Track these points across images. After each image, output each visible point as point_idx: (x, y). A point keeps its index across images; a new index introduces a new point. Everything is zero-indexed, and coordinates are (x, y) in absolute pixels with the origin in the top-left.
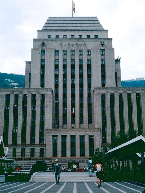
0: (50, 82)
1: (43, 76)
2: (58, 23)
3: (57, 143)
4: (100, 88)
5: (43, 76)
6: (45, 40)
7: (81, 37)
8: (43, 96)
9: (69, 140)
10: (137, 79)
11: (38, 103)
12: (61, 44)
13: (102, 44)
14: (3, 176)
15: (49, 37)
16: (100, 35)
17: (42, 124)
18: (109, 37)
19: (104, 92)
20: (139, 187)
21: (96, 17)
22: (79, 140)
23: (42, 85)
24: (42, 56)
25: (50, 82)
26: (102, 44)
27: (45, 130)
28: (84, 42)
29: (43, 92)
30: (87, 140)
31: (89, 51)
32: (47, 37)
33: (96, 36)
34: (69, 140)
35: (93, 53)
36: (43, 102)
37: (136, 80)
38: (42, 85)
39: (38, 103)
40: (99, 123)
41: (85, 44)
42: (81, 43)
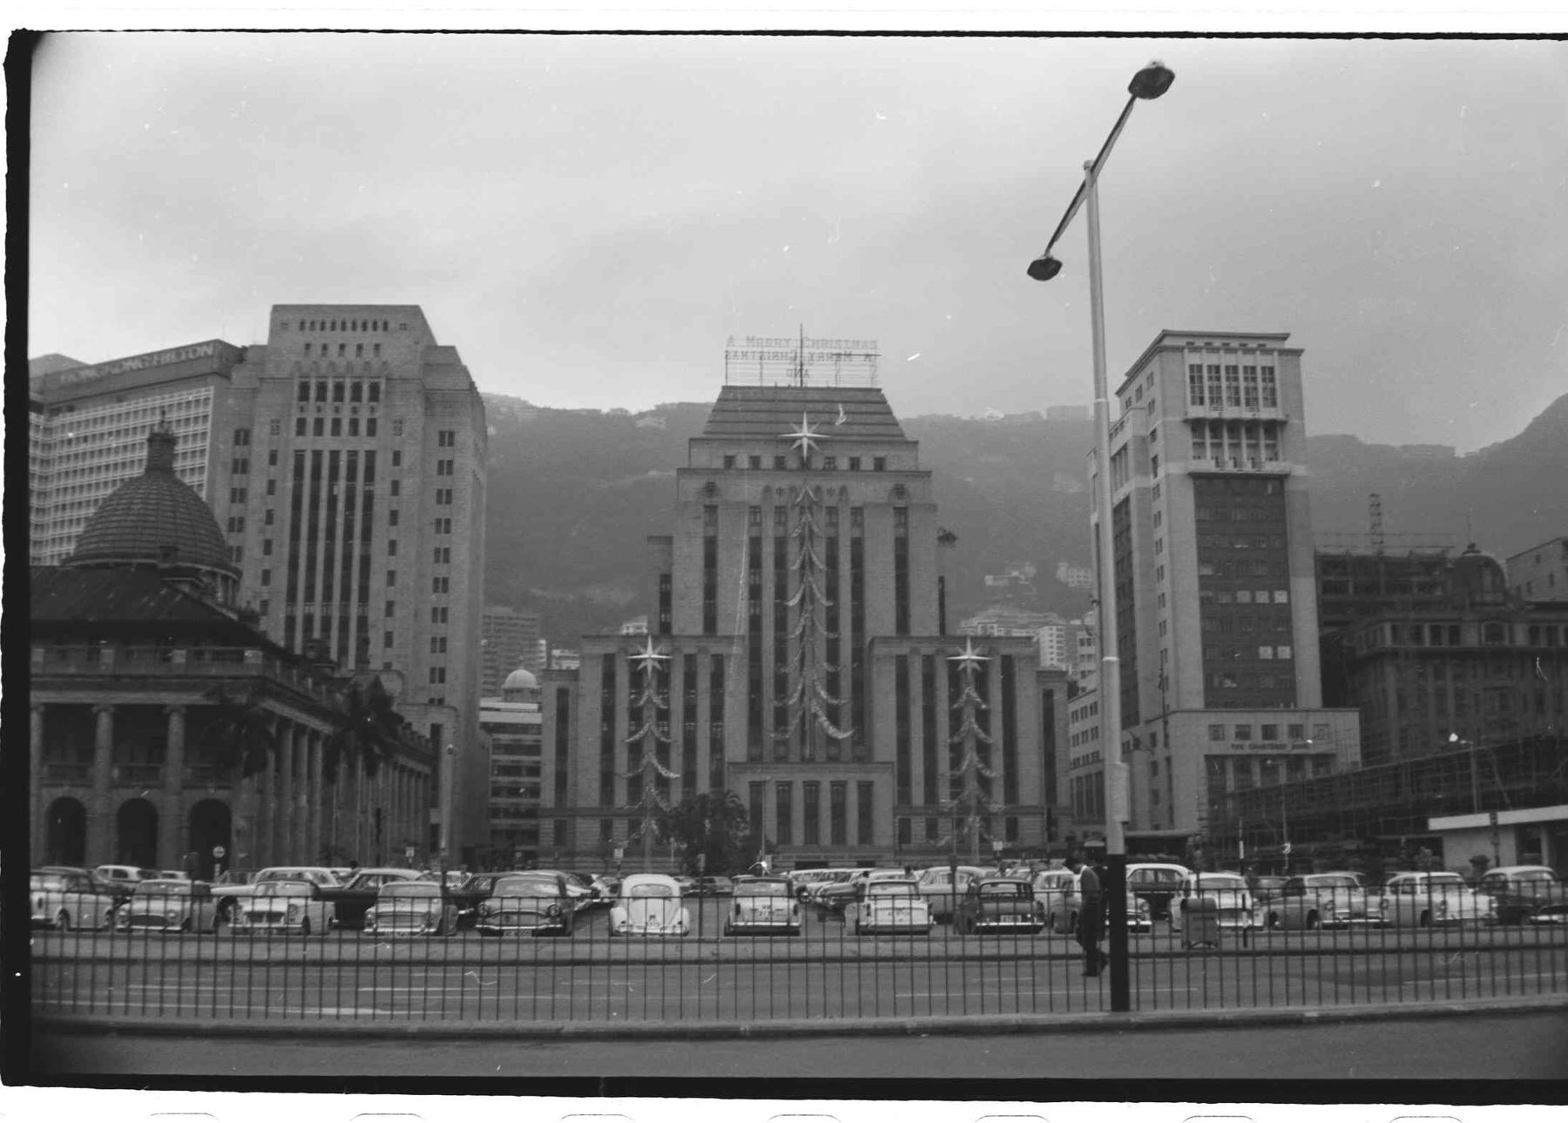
0: (735, 610)
1: (710, 591)
2: (756, 408)
3: (327, 539)
4: (891, 638)
5: (710, 591)
6: (716, 471)
7: (829, 463)
8: (719, 661)
9: (798, 796)
10: (1049, 411)
11: (704, 682)
12: (767, 490)
13: (900, 491)
14: (922, 909)
15: (729, 461)
16: (897, 460)
17: (717, 746)
18: (922, 468)
19: (904, 649)
20: (59, 688)
21: (879, 390)
22: (829, 796)
23: (710, 622)
24: (707, 524)
25: (735, 610)
26: (900, 491)
27: (726, 765)
28: (840, 484)
29: (715, 649)
30: (853, 797)
31: (857, 512)
32: (719, 463)
33: (880, 465)
34: (798, 796)
35: (869, 520)
36: (718, 680)
37: (1045, 417)
38: (710, 622)
39: (704, 682)
40: (753, 339)
41: (843, 490)
42: (836, 484)
